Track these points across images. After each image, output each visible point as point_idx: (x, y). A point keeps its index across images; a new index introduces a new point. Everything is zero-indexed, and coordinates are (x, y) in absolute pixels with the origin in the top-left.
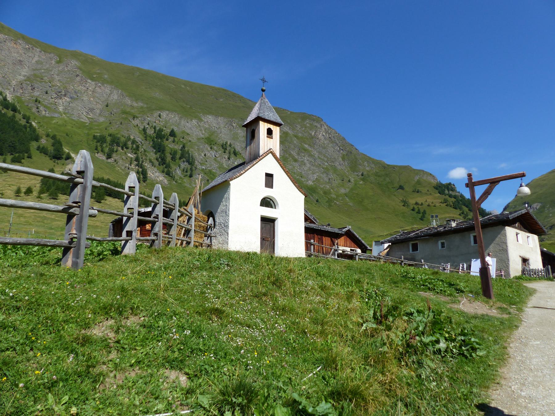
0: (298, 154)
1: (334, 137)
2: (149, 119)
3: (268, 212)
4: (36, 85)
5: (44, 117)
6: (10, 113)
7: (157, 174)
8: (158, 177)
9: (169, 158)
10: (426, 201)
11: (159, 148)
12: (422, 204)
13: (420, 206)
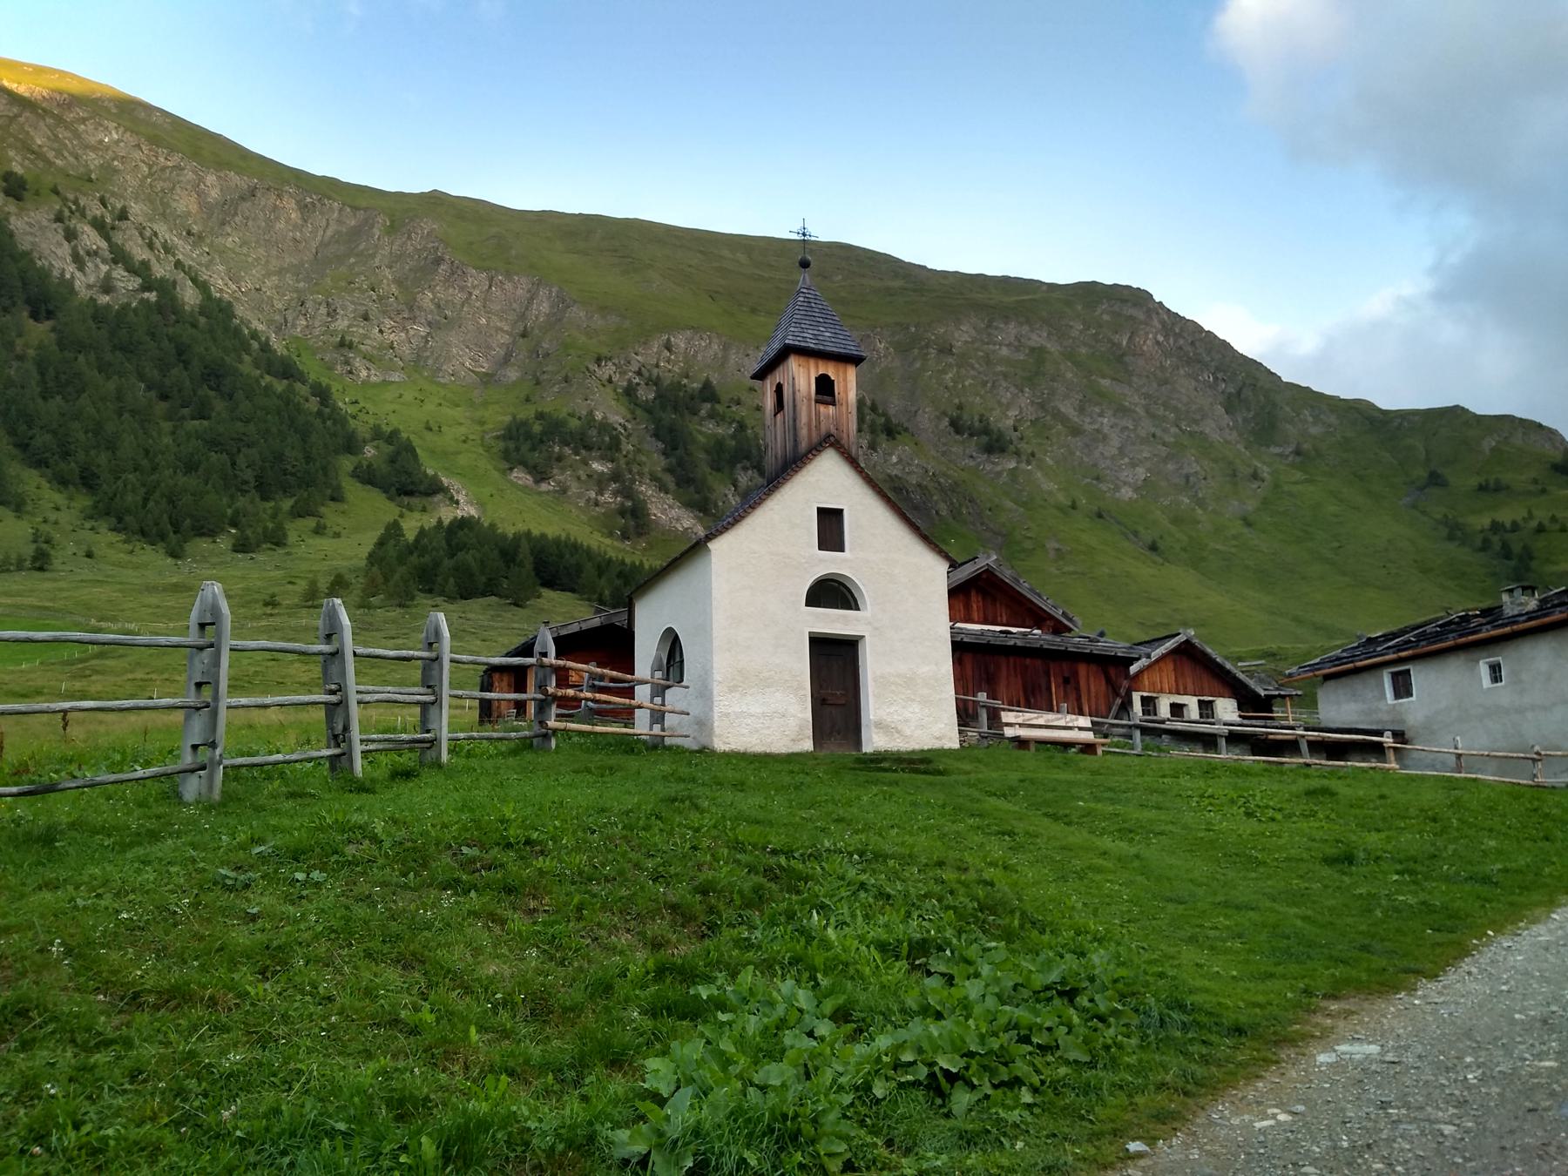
0: (1081, 410)
1: (1192, 343)
2: (639, 358)
3: (833, 622)
4: (338, 303)
5: (366, 383)
6: (280, 386)
7: (675, 512)
8: (678, 520)
9: (704, 469)
10: (1531, 516)
11: (672, 440)
12: (1515, 527)
13: (1508, 536)
